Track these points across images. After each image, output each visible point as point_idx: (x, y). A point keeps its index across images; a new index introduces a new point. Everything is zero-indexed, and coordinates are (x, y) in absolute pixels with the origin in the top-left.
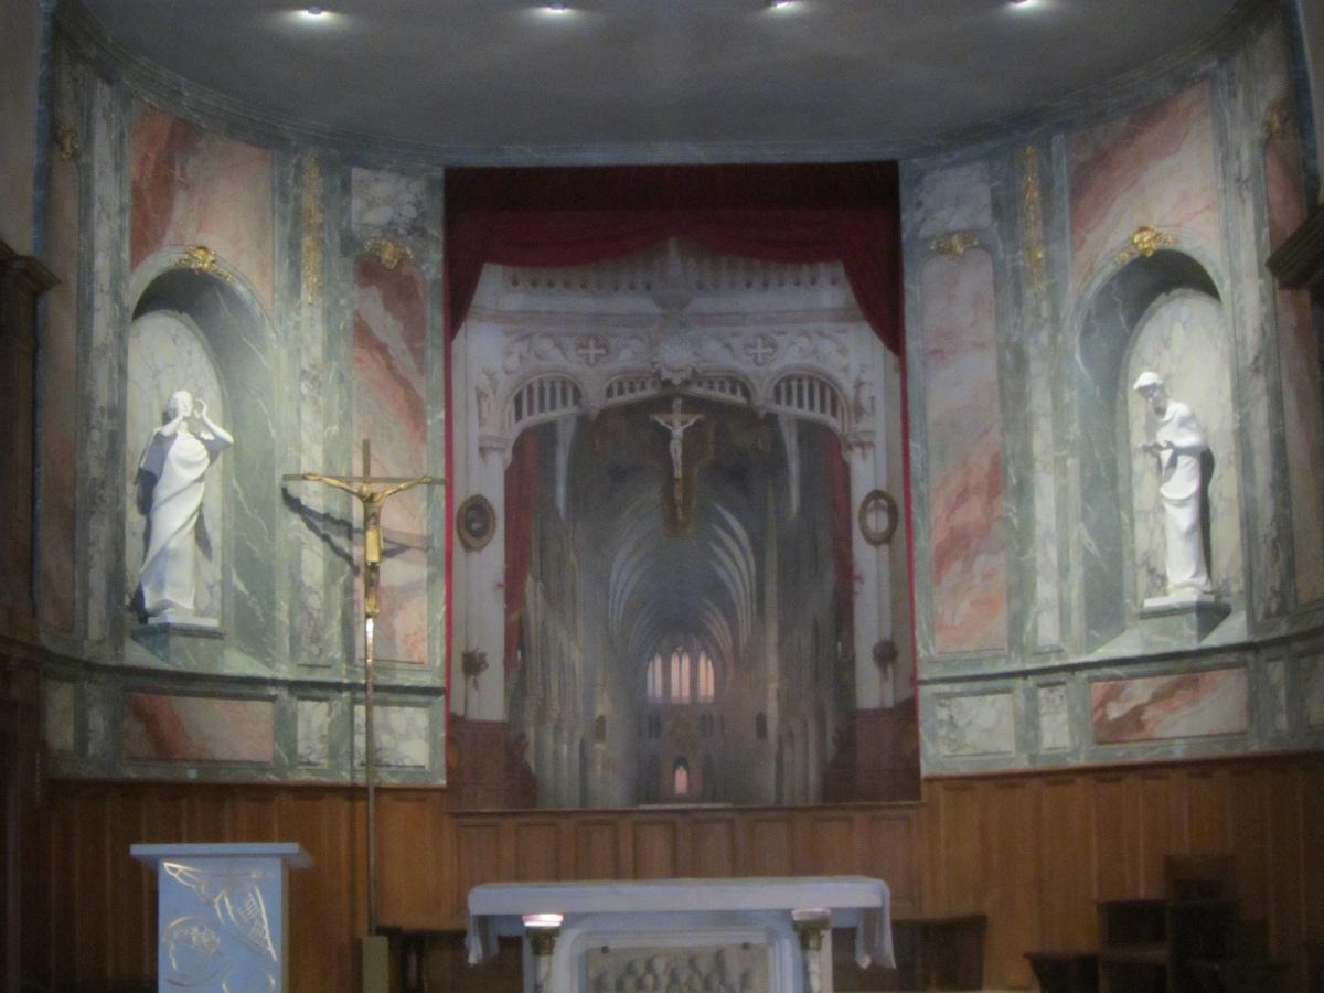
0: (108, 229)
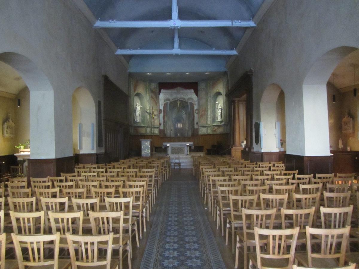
0: (132, 91)
